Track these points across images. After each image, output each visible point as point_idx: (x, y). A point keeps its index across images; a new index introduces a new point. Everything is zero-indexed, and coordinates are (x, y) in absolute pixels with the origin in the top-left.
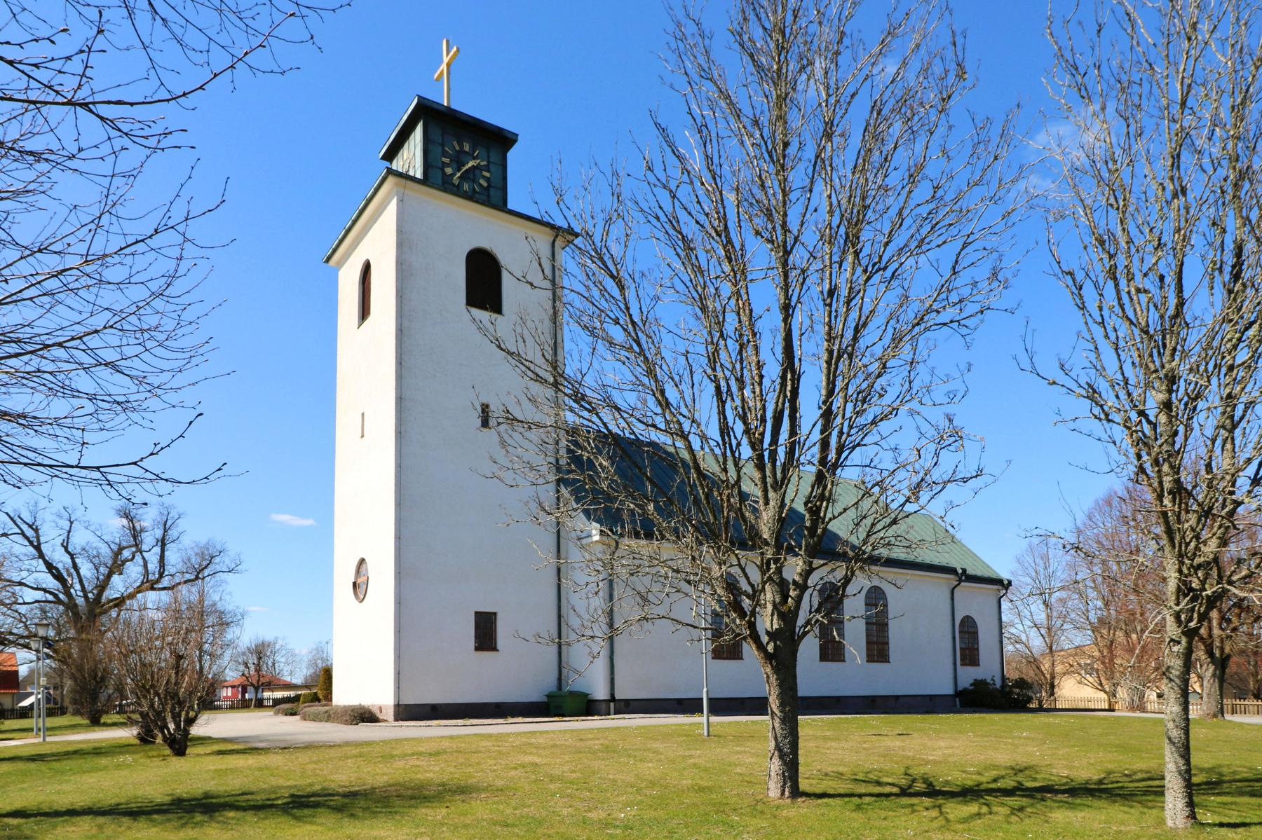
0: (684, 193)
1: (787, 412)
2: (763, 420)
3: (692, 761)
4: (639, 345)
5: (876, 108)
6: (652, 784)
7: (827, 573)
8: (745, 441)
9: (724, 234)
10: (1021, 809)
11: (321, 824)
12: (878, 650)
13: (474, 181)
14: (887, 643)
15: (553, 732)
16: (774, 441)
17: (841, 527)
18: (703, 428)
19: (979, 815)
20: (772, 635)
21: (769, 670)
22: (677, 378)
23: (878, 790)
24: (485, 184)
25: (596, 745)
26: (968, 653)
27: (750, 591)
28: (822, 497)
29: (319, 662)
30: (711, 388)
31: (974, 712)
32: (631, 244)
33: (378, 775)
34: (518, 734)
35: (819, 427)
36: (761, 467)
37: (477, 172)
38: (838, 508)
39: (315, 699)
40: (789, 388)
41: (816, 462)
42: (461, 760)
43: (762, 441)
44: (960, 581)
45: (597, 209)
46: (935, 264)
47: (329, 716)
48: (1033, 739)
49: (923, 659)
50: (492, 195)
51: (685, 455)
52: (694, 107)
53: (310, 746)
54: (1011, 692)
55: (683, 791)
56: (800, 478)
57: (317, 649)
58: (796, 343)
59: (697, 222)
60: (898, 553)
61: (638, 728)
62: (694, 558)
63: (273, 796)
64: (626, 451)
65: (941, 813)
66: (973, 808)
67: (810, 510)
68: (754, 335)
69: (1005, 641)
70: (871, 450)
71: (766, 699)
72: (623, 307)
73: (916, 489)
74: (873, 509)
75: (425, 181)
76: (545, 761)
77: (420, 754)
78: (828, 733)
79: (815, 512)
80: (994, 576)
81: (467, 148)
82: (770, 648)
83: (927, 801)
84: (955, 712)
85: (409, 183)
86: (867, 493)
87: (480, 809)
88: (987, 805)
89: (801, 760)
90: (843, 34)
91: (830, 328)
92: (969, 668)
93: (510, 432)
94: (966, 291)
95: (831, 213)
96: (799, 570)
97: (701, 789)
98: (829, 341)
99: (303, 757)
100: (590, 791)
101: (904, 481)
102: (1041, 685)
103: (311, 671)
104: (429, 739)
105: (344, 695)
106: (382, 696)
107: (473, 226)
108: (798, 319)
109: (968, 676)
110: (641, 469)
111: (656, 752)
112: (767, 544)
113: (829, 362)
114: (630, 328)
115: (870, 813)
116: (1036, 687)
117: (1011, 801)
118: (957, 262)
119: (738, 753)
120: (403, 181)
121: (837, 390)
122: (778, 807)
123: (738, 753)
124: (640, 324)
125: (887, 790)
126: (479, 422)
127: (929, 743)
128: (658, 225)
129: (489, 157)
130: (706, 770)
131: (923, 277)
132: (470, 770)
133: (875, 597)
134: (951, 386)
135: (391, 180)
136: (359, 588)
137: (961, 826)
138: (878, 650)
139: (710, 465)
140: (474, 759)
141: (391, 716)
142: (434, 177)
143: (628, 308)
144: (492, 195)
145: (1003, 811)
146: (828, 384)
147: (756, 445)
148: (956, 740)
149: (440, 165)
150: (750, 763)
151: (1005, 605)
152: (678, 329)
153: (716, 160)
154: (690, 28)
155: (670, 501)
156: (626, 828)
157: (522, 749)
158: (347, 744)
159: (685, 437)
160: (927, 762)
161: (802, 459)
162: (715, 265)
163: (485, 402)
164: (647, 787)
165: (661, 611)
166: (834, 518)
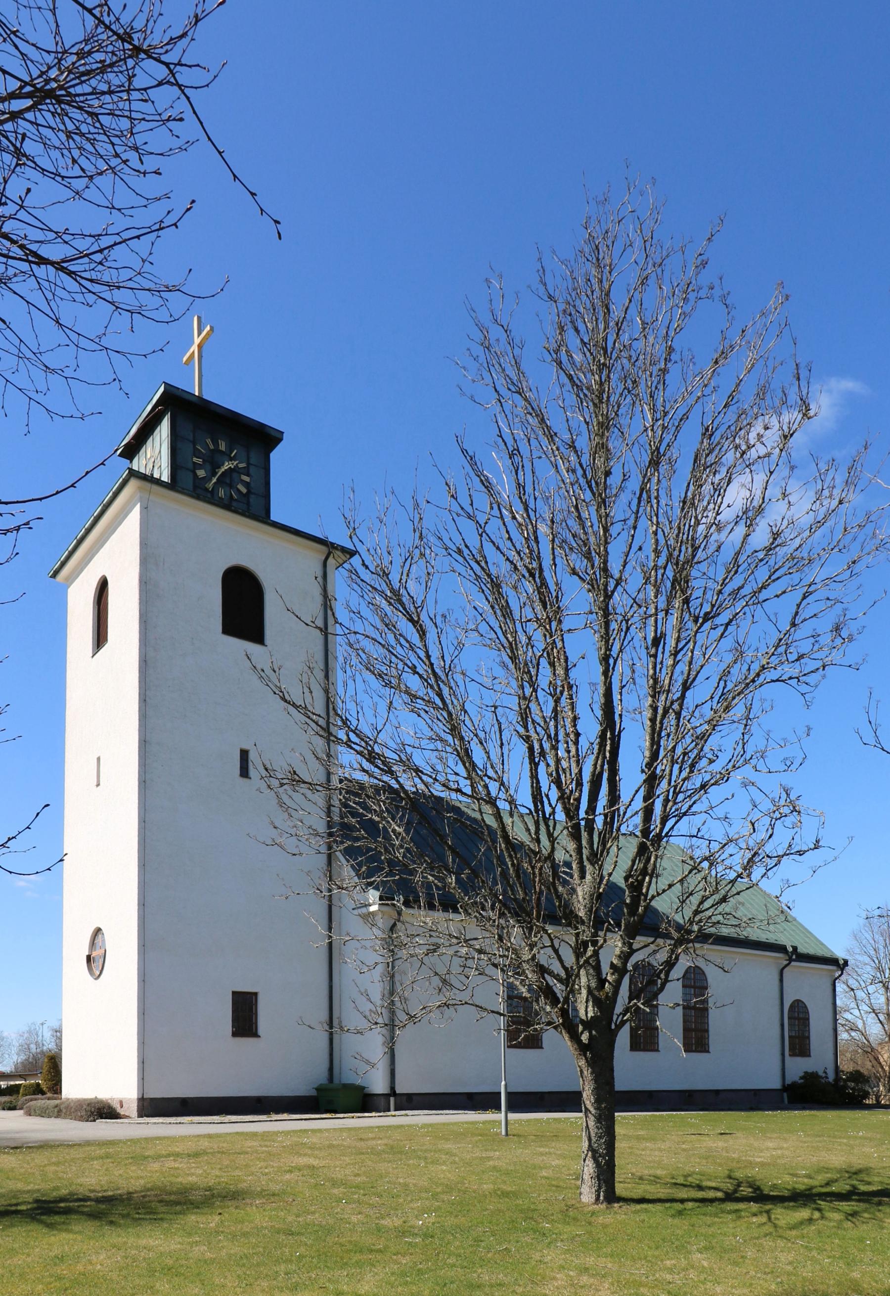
0: (494, 528)
1: (605, 775)
2: (580, 784)
3: (491, 1163)
4: (438, 691)
5: (707, 433)
6: (449, 1189)
7: (651, 952)
8: (559, 808)
9: (536, 574)
10: (854, 1214)
11: (80, 1232)
12: (696, 1038)
13: (231, 486)
14: (707, 1031)
15: (327, 1130)
16: (591, 809)
17: (664, 904)
18: (512, 792)
19: (810, 1220)
20: (588, 1025)
21: (582, 1063)
22: (482, 735)
23: (700, 1195)
24: (244, 490)
25: (380, 1144)
26: (798, 1039)
27: (563, 974)
28: (644, 872)
29: (33, 1047)
30: (523, 748)
31: (804, 1109)
32: (433, 585)
33: (131, 1178)
34: (287, 1133)
35: (642, 793)
36: (575, 835)
37: (235, 475)
38: (663, 883)
39: (37, 1090)
40: (608, 748)
41: (638, 834)
42: (226, 1163)
43: (578, 808)
44: (790, 960)
45: (394, 543)
46: (773, 618)
47: (60, 1111)
48: (871, 1140)
49: (745, 1046)
50: (253, 504)
51: (491, 821)
52: (506, 430)
53: (44, 1146)
54: (845, 1087)
55: (485, 1196)
56: (619, 849)
57: (30, 1032)
58: (616, 697)
59: (508, 559)
60: (725, 931)
61: (425, 1126)
62: (501, 938)
63: (14, 1201)
64: (427, 815)
65: (769, 1218)
66: (804, 1213)
67: (631, 887)
68: (570, 687)
69: (840, 1029)
70: (697, 820)
71: (579, 1094)
72: (422, 654)
73: (748, 866)
74: (701, 885)
75: (174, 485)
76: (323, 1163)
77: (177, 1155)
78: (641, 1133)
79: (636, 888)
80: (828, 955)
81: (223, 446)
82: (585, 1038)
83: (754, 1207)
84: (782, 1109)
85: (155, 488)
86: (695, 868)
87: (257, 1216)
88: (819, 1210)
89: (617, 1162)
90: (671, 350)
91: (656, 681)
92: (799, 1059)
93: (290, 792)
94: (805, 647)
95: (657, 552)
96: (617, 951)
97: (505, 1194)
98: (653, 696)
99: (40, 1158)
100: (380, 1196)
101: (736, 859)
102: (879, 1079)
103: (23, 1057)
104: (183, 1139)
105: (76, 1086)
106: (121, 1085)
107: (232, 541)
108: (621, 670)
109: (798, 1067)
110: (443, 838)
111: (448, 1153)
112: (583, 923)
113: (653, 720)
114: (432, 681)
115: (694, 1219)
116: (873, 1081)
117: (846, 1206)
118: (797, 613)
119: (542, 1154)
120: (147, 485)
121: (662, 753)
122: (593, 1213)
123: (542, 1154)
124: (443, 677)
125: (711, 1194)
126: (238, 771)
127: (756, 1144)
128: (461, 559)
129: (248, 459)
130: (507, 1173)
131: (757, 632)
132: (237, 1173)
133: (695, 982)
134: (787, 752)
135: (133, 484)
136: (94, 962)
137: (794, 1233)
138: (696, 1038)
139: (519, 833)
140: (241, 1160)
141: (133, 1112)
142: (184, 480)
143: (428, 657)
144: (253, 504)
145: (837, 1216)
146: (652, 745)
147: (571, 812)
148: (785, 1139)
149: (190, 466)
150: (557, 1166)
151: (840, 987)
152: (485, 683)
153: (529, 489)
154: (495, 332)
155: (475, 873)
156: (426, 1236)
157: (296, 1149)
158: (88, 1143)
159: (492, 802)
160: (751, 1165)
161: (623, 829)
162: (521, 596)
163: (245, 747)
164: (444, 1192)
165: (465, 996)
166: (658, 894)
